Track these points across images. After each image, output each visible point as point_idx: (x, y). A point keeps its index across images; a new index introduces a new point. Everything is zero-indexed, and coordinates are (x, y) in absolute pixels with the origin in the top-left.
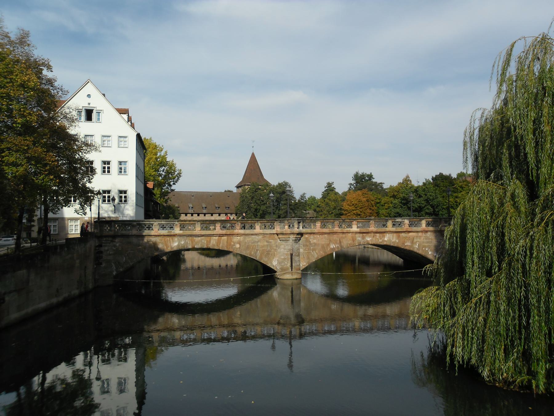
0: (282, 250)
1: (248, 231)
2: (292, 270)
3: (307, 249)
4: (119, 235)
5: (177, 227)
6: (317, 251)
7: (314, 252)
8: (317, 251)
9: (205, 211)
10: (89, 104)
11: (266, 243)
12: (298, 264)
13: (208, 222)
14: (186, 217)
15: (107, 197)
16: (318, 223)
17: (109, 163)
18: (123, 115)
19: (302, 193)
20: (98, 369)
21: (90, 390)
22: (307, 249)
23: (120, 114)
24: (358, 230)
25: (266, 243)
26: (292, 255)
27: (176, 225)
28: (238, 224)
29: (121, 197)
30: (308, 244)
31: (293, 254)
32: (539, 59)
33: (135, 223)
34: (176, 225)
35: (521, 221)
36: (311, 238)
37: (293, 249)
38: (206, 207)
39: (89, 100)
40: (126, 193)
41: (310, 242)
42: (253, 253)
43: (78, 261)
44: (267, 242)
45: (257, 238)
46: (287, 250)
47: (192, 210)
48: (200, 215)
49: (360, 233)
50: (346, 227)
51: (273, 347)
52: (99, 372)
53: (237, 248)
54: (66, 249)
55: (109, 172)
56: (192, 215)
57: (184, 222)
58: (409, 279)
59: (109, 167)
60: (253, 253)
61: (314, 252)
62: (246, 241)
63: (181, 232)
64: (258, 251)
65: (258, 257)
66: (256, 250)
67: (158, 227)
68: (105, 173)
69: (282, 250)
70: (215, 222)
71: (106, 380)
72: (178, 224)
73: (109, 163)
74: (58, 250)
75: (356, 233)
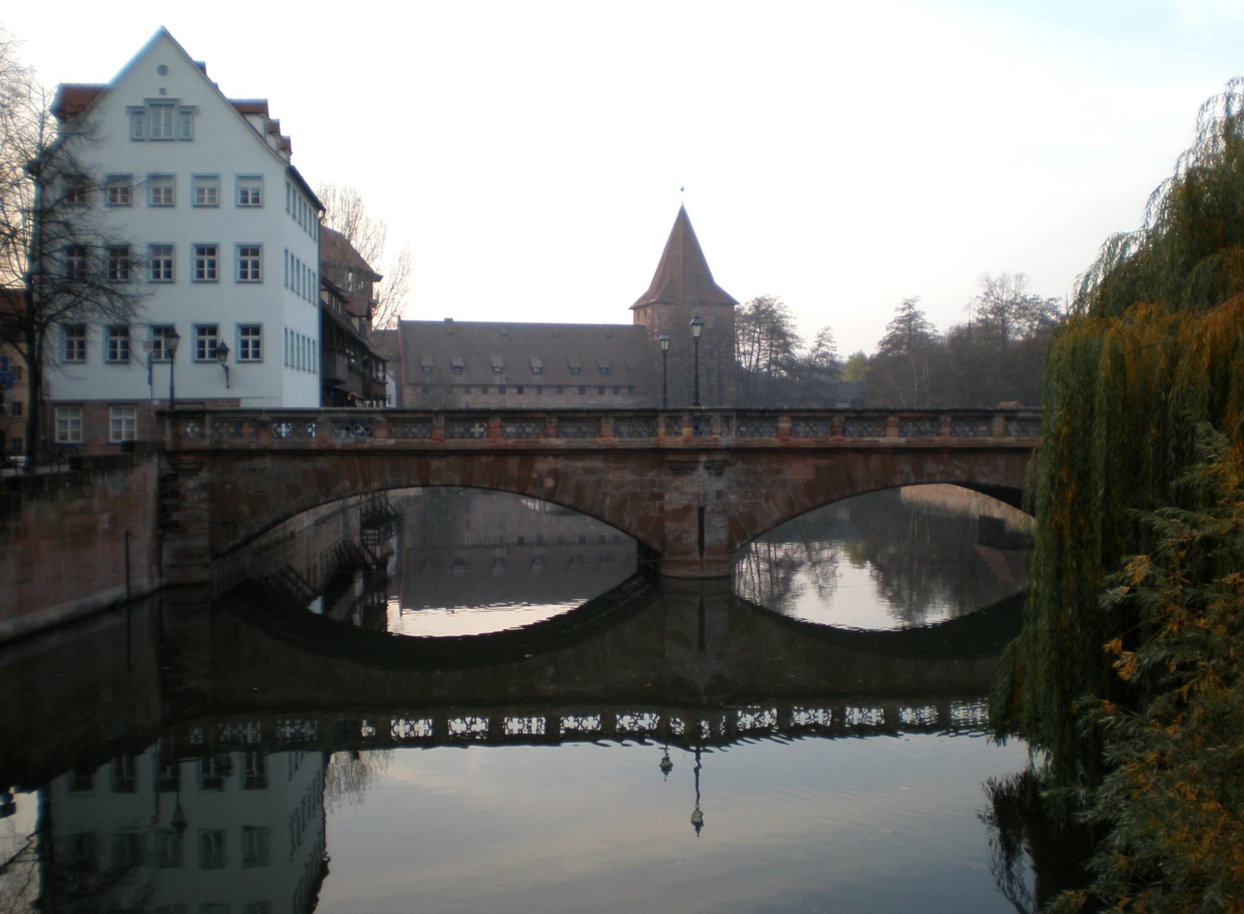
3: (749, 495)
7: (771, 502)
9: (538, 379)
14: (485, 396)
20: (158, 812)
21: (961, 610)
22: (749, 495)
27: (378, 422)
28: (550, 422)
31: (708, 509)
33: (264, 417)
38: (608, 370)
39: (161, 82)
43: (105, 517)
48: (525, 390)
51: (666, 767)
52: (179, 810)
56: (502, 389)
61: (771, 502)
64: (608, 499)
72: (381, 419)
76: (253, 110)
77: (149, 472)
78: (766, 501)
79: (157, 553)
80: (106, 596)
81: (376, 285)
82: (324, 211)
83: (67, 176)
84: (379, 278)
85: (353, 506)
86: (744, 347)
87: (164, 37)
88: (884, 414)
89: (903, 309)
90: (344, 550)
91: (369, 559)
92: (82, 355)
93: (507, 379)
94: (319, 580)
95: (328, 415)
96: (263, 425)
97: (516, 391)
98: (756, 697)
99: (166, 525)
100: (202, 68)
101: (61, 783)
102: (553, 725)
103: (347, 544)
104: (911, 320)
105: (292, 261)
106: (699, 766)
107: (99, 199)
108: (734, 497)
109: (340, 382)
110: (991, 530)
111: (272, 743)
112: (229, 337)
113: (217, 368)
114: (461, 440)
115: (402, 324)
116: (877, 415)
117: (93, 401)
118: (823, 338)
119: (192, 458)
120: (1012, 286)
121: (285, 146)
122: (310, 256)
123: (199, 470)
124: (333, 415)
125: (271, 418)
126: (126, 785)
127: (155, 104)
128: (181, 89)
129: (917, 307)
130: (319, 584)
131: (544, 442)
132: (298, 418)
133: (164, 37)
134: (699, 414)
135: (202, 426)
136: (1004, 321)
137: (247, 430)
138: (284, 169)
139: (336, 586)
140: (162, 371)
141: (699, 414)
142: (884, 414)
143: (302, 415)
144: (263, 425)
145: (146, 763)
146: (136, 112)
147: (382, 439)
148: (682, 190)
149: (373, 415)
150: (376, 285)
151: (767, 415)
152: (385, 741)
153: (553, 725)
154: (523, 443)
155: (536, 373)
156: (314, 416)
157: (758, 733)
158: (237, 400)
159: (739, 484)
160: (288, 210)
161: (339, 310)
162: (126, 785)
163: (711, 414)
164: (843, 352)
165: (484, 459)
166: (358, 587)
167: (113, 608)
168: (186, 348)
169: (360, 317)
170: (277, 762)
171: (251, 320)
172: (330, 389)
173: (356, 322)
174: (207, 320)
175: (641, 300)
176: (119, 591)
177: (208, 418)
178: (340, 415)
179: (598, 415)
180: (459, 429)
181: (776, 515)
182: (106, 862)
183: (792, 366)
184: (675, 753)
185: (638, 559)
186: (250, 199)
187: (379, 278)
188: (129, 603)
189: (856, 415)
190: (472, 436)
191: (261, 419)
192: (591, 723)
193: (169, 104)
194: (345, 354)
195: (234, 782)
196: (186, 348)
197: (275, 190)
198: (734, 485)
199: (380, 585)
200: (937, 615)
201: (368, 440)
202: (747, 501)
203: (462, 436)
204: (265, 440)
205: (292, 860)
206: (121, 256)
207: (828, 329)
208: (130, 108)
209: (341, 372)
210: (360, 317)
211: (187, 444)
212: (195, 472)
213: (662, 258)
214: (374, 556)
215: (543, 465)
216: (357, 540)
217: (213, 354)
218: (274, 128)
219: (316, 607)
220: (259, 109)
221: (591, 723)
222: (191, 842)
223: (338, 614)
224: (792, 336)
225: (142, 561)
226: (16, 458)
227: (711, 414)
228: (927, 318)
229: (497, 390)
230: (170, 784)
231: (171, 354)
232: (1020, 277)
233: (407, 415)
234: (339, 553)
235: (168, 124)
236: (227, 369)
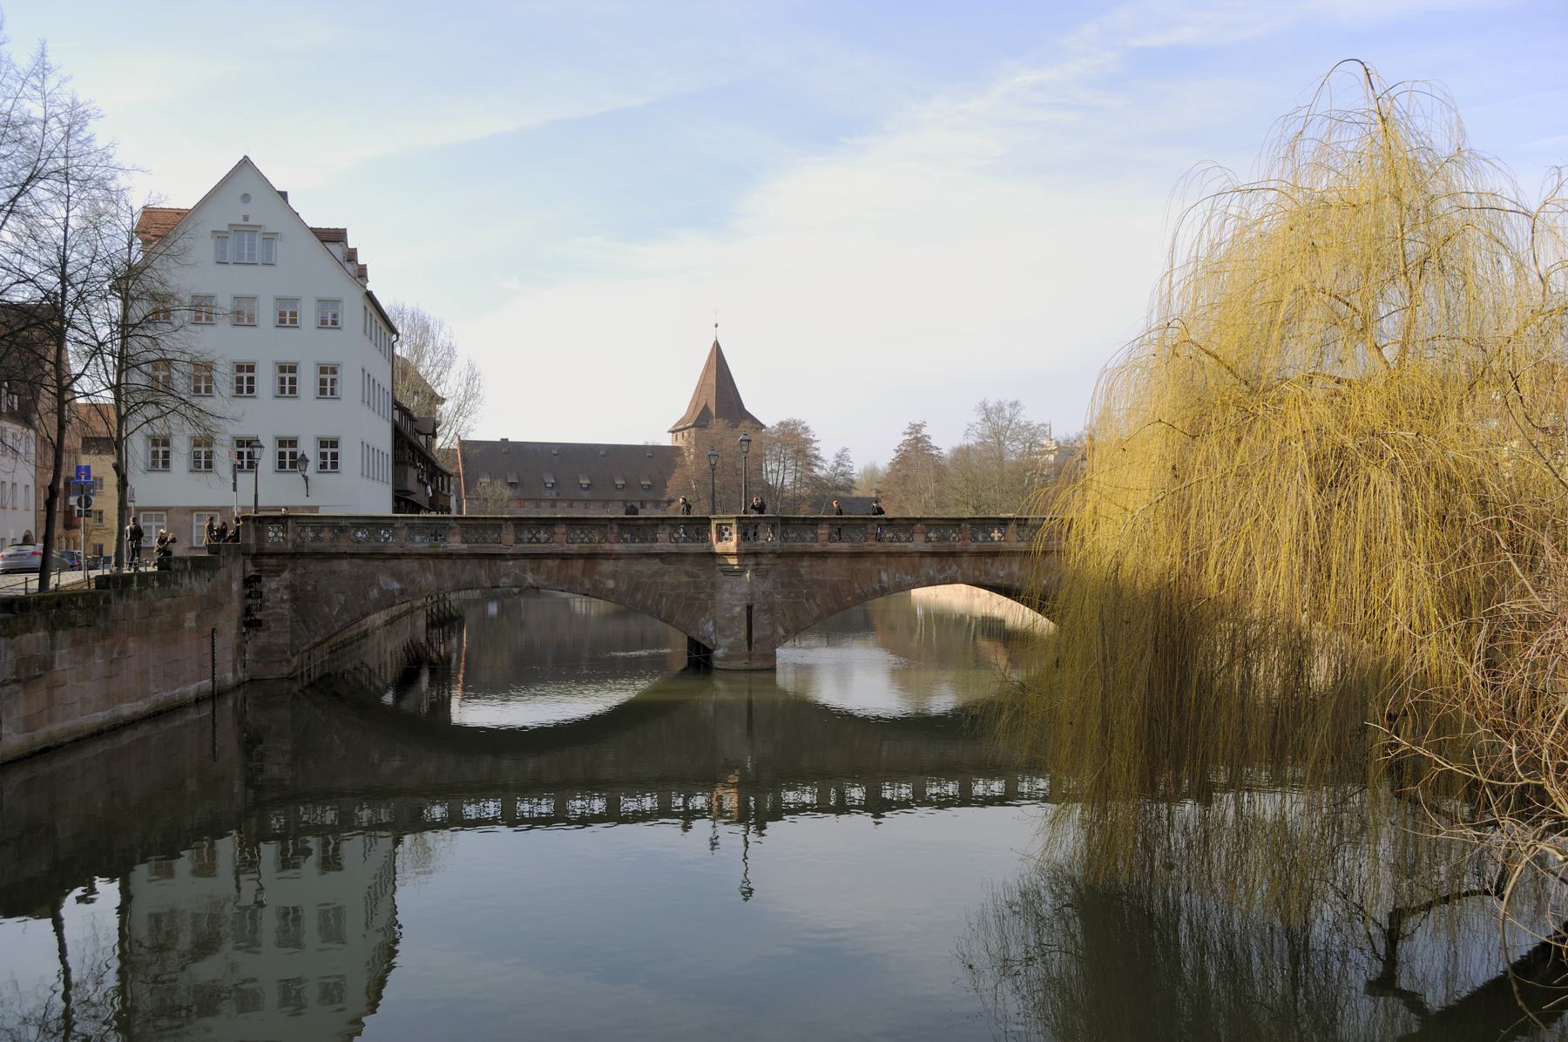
0: (726, 595)
2: (750, 649)
4: (306, 551)
5: (454, 534)
6: (819, 601)
7: (811, 601)
8: (819, 601)
9: (586, 494)
10: (246, 218)
11: (684, 579)
12: (768, 632)
13: (532, 522)
15: (203, 455)
16: (822, 528)
17: (293, 369)
18: (329, 245)
19: (838, 450)
23: (322, 241)
24: (928, 547)
25: (684, 579)
26: (749, 608)
27: (451, 528)
28: (611, 528)
29: (323, 455)
31: (755, 607)
33: (344, 523)
34: (451, 528)
36: (802, 567)
37: (752, 595)
40: (295, 446)
41: (802, 576)
42: (649, 602)
44: (687, 573)
46: (739, 597)
47: (554, 493)
49: (933, 554)
50: (586, 540)
54: (156, 584)
55: (251, 390)
59: (295, 379)
60: (649, 602)
61: (811, 601)
63: (465, 546)
64: (664, 599)
66: (657, 597)
68: (242, 392)
69: (726, 595)
70: (550, 522)
71: (293, 908)
73: (293, 369)
74: (135, 586)
75: (923, 554)
76: (332, 237)
77: (234, 572)
78: (807, 600)
79: (240, 650)
80: (191, 690)
81: (440, 408)
82: (398, 335)
83: (154, 297)
84: (443, 400)
85: (418, 608)
86: (771, 466)
87: (245, 162)
89: (911, 433)
90: (411, 646)
91: (434, 656)
92: (166, 464)
93: (557, 494)
94: (390, 675)
96: (342, 529)
98: (797, 779)
99: (250, 623)
100: (284, 195)
101: (141, 872)
103: (414, 642)
105: (368, 379)
107: (182, 316)
109: (410, 493)
110: (993, 628)
111: (346, 824)
112: (308, 448)
113: (296, 478)
114: (528, 545)
115: (463, 444)
116: (905, 522)
117: (177, 507)
118: (841, 458)
119: (273, 561)
121: (362, 273)
122: (384, 378)
123: (283, 571)
124: (409, 521)
126: (206, 869)
127: (236, 229)
128: (260, 214)
129: (925, 431)
130: (389, 680)
131: (607, 547)
132: (373, 523)
133: (245, 162)
134: (747, 521)
135: (285, 531)
136: (1000, 443)
137: (326, 534)
138: (362, 293)
139: (406, 680)
140: (245, 479)
141: (747, 521)
142: (912, 522)
143: (380, 521)
144: (342, 529)
145: (227, 848)
146: (219, 236)
147: (455, 543)
148: (716, 326)
150: (440, 408)
151: (808, 522)
152: (456, 821)
154: (586, 548)
155: (585, 489)
156: (392, 521)
157: (801, 809)
158: (316, 508)
159: (783, 585)
160: (365, 332)
161: (408, 429)
162: (206, 869)
164: (858, 467)
165: (550, 562)
166: (425, 679)
167: (198, 701)
168: (267, 458)
169: (427, 435)
170: (352, 847)
171: (328, 434)
172: (402, 500)
173: (422, 439)
174: (287, 433)
175: (679, 423)
176: (206, 683)
177: (290, 522)
178: (416, 521)
179: (656, 522)
180: (526, 535)
181: (816, 612)
182: (185, 941)
183: (818, 482)
184: (724, 830)
185: (689, 654)
186: (329, 321)
187: (443, 400)
188: (215, 696)
190: (538, 541)
192: (648, 803)
193: (254, 230)
194: (416, 467)
195: (311, 863)
196: (267, 458)
197: (353, 313)
199: (442, 673)
200: (942, 701)
203: (530, 541)
204: (344, 545)
205: (43, 45)
206: (203, 375)
207: (845, 450)
208: (214, 232)
209: (412, 484)
210: (427, 435)
211: (268, 547)
212: (277, 572)
214: (439, 654)
215: (606, 567)
216: (423, 640)
217: (293, 465)
218: (352, 256)
219: (388, 698)
220: (337, 236)
221: (648, 803)
222: (269, 922)
223: (407, 705)
224: (816, 457)
225: (226, 656)
226: (459, 682)
228: (1031, 415)
229: (549, 504)
230: (249, 863)
231: (252, 465)
232: (1014, 405)
234: (407, 650)
235: (252, 247)
236: (306, 479)
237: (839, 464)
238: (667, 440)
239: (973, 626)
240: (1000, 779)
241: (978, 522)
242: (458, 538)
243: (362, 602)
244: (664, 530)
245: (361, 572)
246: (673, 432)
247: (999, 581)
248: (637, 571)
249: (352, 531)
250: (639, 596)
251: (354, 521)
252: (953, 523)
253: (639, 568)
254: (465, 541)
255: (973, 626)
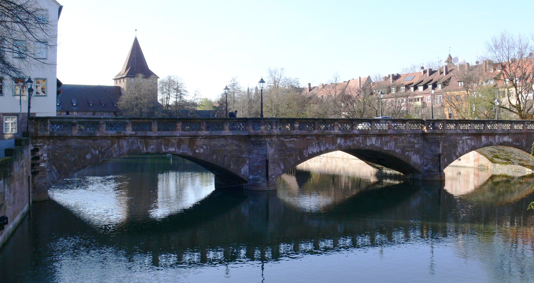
1: (214, 133)
6: (294, 158)
7: (291, 158)
11: (235, 148)
16: (296, 124)
25: (235, 148)
27: (127, 124)
28: (203, 124)
30: (283, 148)
32: (520, 67)
34: (127, 124)
35: (523, 88)
41: (287, 146)
45: (222, 142)
53: (201, 153)
57: (137, 121)
58: (25, 138)
61: (291, 158)
62: (212, 145)
64: (226, 157)
65: (226, 164)
67: (104, 126)
78: (289, 158)
88: (333, 121)
93: (62, 108)
95: (105, 120)
97: (66, 113)
102: (335, 244)
104: (234, 86)
106: (262, 276)
108: (276, 156)
120: (279, 72)
125: (78, 121)
129: (237, 80)
142: (333, 121)
149: (125, 120)
153: (316, 247)
156: (98, 120)
159: (279, 151)
163: (272, 121)
189: (323, 121)
191: (73, 122)
198: (277, 151)
201: (123, 132)
202: (282, 158)
213: (145, 59)
227: (272, 121)
233: (141, 121)
237: (195, 95)
238: (111, 83)
239: (432, 173)
240: (47, 192)
241: (303, 121)
242: (131, 128)
243: (83, 161)
244: (226, 124)
245: (82, 146)
246: (115, 80)
247: (367, 148)
248: (214, 144)
249: (78, 125)
250: (215, 157)
251: (80, 120)
252: (345, 121)
253: (214, 143)
254: (134, 130)
255: (432, 173)
